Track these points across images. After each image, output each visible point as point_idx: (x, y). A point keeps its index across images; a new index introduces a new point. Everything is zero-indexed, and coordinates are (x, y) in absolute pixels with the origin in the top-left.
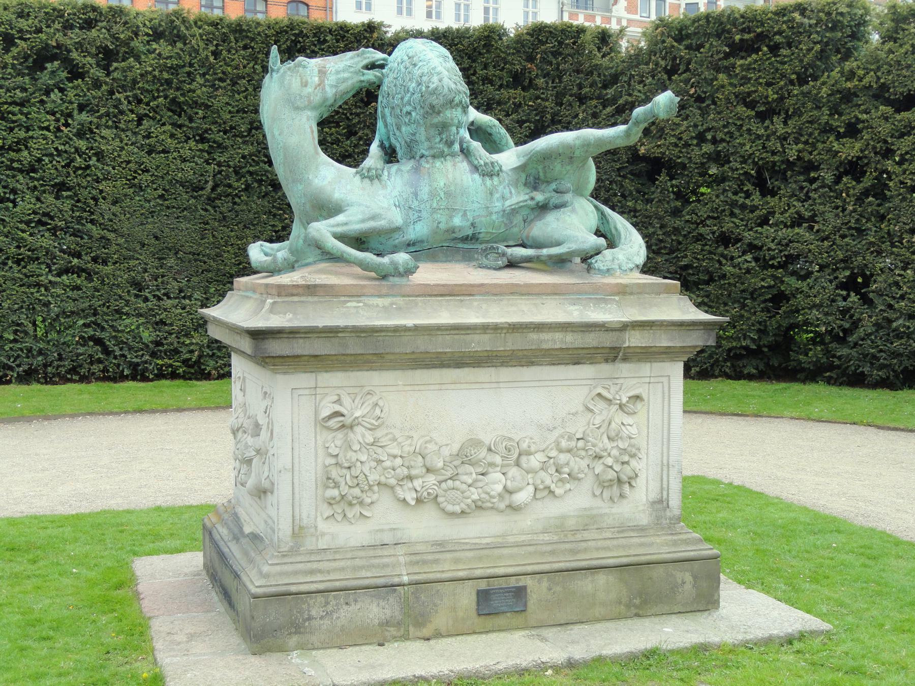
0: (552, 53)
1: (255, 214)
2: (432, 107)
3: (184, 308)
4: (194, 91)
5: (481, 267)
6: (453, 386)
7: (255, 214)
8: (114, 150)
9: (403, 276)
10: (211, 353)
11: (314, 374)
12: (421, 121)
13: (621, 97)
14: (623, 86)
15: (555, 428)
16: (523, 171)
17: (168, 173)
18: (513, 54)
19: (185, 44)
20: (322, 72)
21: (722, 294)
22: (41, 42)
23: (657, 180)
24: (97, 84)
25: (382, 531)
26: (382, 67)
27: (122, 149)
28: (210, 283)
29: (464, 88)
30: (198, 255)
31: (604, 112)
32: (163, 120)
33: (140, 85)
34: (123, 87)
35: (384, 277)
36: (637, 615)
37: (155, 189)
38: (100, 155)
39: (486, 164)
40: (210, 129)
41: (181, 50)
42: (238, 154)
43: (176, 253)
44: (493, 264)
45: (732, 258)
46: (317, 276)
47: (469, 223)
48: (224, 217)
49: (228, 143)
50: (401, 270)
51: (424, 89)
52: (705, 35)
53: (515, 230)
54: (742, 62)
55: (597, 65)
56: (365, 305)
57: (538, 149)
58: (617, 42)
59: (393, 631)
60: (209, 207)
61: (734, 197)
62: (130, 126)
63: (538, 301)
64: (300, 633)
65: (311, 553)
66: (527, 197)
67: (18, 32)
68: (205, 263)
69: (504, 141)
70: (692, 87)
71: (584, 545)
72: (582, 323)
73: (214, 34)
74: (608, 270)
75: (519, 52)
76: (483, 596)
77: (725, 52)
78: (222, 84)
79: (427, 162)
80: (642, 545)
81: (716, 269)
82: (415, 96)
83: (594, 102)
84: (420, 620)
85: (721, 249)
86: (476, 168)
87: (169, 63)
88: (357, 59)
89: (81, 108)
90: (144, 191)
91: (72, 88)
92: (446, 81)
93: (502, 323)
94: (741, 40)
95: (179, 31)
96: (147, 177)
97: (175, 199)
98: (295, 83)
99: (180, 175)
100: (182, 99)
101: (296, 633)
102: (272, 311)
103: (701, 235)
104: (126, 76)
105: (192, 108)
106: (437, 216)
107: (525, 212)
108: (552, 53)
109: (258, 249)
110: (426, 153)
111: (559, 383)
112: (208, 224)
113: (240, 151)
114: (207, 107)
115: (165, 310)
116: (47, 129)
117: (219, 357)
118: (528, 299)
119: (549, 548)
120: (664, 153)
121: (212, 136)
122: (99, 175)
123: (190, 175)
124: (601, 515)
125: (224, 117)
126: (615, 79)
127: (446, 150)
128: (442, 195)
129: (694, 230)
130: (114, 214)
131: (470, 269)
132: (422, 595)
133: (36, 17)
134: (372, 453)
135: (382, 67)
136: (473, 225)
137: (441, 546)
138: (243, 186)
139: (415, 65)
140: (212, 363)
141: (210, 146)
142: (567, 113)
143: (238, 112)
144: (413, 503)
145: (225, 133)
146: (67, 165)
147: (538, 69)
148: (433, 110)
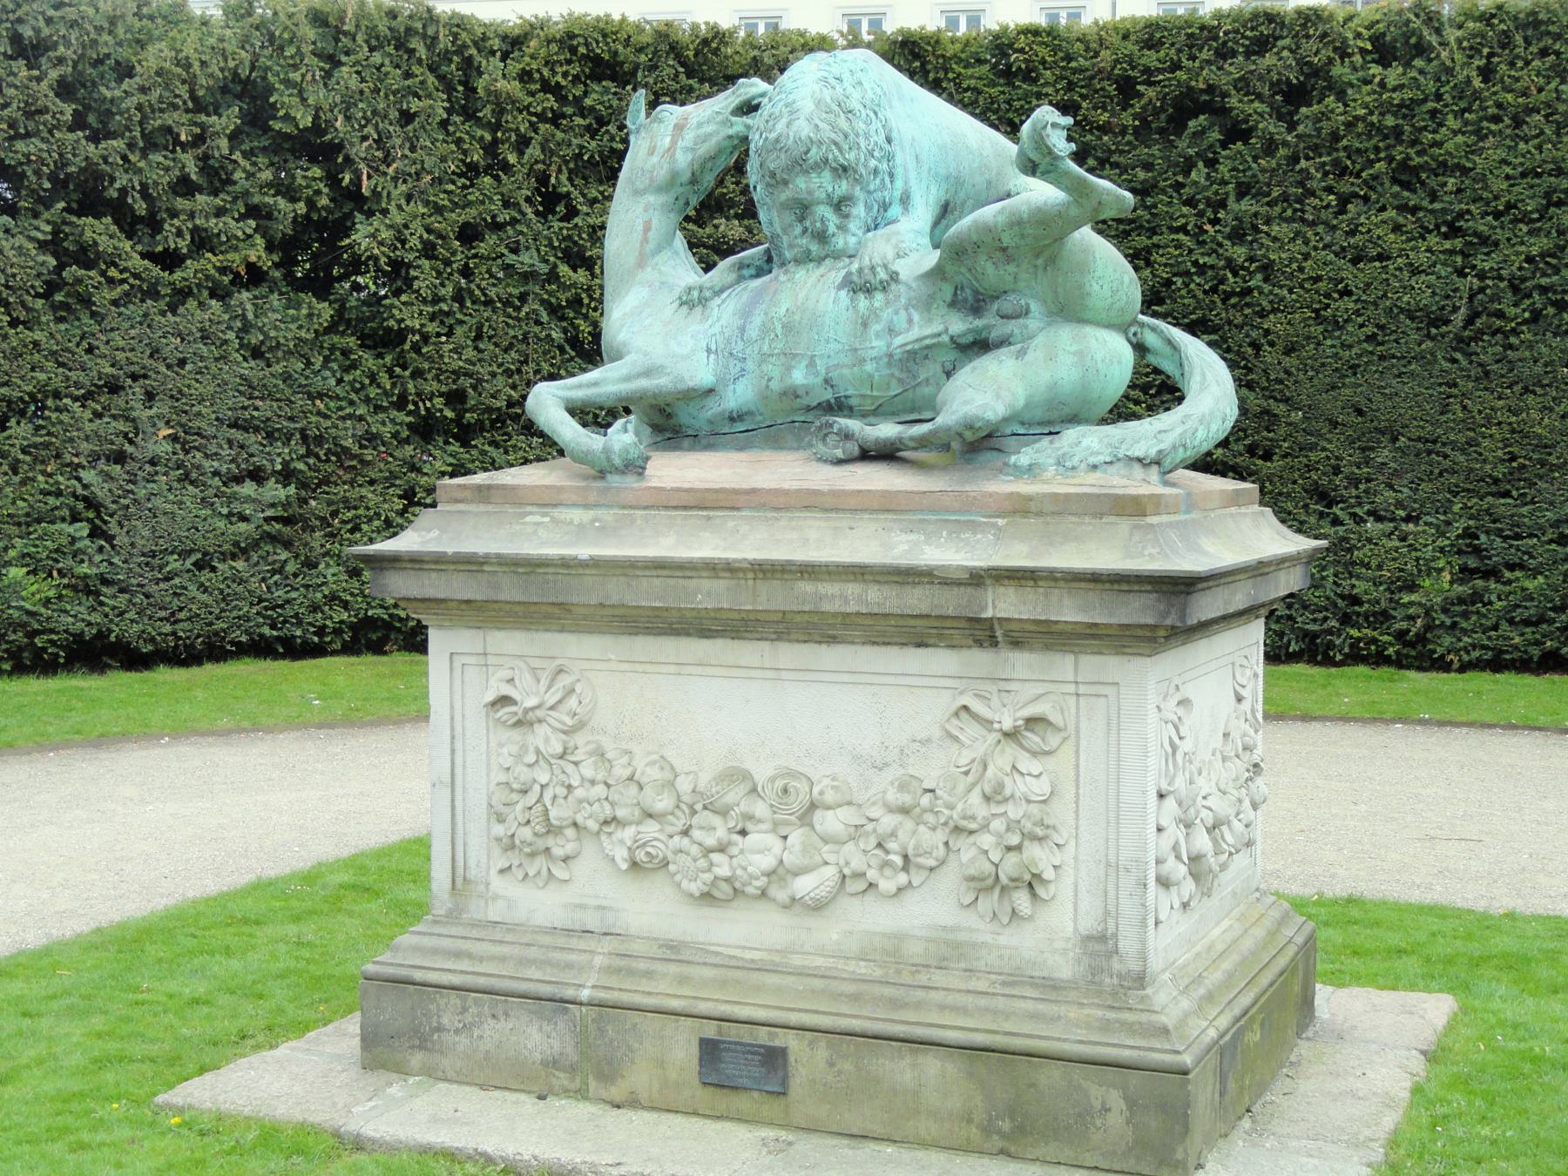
1: (1546, 365)
3: (1403, 539)
4: (1439, 144)
6: (699, 670)
7: (1546, 365)
8: (1291, 260)
10: (1448, 622)
11: (481, 632)
15: (886, 765)
17: (1385, 295)
22: (1179, 84)
24: (1270, 147)
25: (583, 907)
27: (1306, 256)
28: (1456, 494)
30: (1434, 442)
33: (1345, 142)
34: (1316, 148)
35: (602, 474)
36: (1003, 1152)
37: (1361, 326)
38: (1267, 269)
40: (1468, 212)
42: (1518, 254)
43: (1395, 439)
44: (839, 453)
47: (819, 380)
48: (1487, 374)
49: (1500, 235)
50: (617, 461)
53: (927, 390)
56: (554, 520)
59: (562, 1079)
60: (1458, 356)
62: (1324, 215)
64: (426, 1049)
65: (475, 924)
68: (1446, 456)
71: (920, 994)
73: (1483, 37)
74: (1030, 468)
76: (710, 1050)
78: (1493, 127)
80: (1034, 1016)
84: (608, 1072)
87: (1397, 97)
89: (1243, 191)
90: (1341, 328)
91: (1227, 158)
93: (739, 561)
96: (1349, 304)
97: (1396, 341)
101: (420, 1048)
104: (1319, 130)
111: (891, 680)
112: (1455, 385)
113: (1523, 248)
114: (1465, 171)
115: (1369, 540)
116: (1183, 229)
117: (1464, 631)
119: (850, 988)
122: (1264, 303)
124: (974, 945)
125: (1495, 188)
127: (814, 247)
128: (779, 331)
130: (1288, 372)
132: (609, 1028)
133: (1173, 44)
134: (557, 771)
136: (827, 381)
137: (673, 950)
138: (1527, 315)
140: (1447, 640)
143: (1523, 175)
144: (624, 866)
145: (1496, 218)
146: (1214, 290)
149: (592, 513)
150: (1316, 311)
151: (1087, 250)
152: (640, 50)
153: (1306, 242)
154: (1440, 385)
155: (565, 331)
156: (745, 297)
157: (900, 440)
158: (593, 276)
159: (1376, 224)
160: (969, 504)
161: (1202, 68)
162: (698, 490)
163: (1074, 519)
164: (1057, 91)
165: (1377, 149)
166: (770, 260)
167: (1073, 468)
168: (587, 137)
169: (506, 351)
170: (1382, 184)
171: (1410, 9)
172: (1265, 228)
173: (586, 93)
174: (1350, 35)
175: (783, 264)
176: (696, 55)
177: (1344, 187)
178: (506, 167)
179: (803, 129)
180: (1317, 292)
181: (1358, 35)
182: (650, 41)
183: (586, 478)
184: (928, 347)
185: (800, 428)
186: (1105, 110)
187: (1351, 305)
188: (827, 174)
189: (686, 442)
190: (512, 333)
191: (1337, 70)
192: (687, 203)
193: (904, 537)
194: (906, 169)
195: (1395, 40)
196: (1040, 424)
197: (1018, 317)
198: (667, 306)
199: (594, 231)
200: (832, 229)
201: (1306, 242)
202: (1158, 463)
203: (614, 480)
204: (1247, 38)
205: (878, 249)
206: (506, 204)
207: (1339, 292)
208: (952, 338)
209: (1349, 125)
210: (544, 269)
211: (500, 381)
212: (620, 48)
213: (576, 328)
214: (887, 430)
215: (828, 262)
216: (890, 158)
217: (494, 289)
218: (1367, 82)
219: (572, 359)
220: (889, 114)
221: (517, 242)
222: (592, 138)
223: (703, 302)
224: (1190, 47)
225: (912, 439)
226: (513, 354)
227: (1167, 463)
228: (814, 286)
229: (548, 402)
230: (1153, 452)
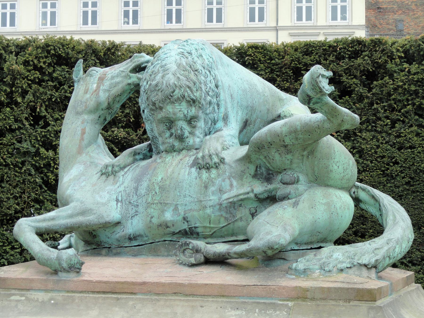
8: (372, 148)
16: (250, 162)
17: (413, 164)
27: (378, 147)
33: (393, 97)
34: (381, 99)
35: (56, 272)
37: (403, 178)
44: (193, 260)
47: (180, 218)
50: (65, 265)
53: (240, 224)
56: (27, 299)
62: (385, 128)
67: (304, 66)
74: (305, 271)
90: (394, 179)
104: (382, 91)
118: (188, 301)
127: (177, 144)
133: (317, 54)
149: (50, 295)
150: (383, 171)
151: (330, 146)
152: (79, 52)
153: (378, 141)
155: (42, 178)
156: (138, 171)
157: (228, 254)
158: (56, 153)
159: (409, 133)
160: (272, 293)
161: (330, 64)
163: (333, 303)
164: (266, 73)
165: (408, 100)
166: (151, 150)
167: (330, 271)
168: (54, 91)
169: (15, 187)
170: (410, 115)
171: (420, 40)
172: (359, 134)
173: (54, 71)
174: (394, 51)
175: (159, 153)
176: (104, 55)
177: (394, 116)
178: (17, 104)
179: (171, 79)
180: (383, 163)
181: (398, 50)
182: (84, 48)
183: (47, 273)
184: (242, 200)
185: (169, 244)
186: (287, 82)
187: (399, 169)
188: (184, 104)
189: (104, 251)
190: (17, 179)
191: (389, 66)
192: (105, 120)
193: (233, 313)
194: (226, 102)
195: (414, 53)
196: (306, 244)
197: (293, 183)
198: (94, 175)
199: (57, 133)
200: (186, 134)
201: (378, 141)
202: (375, 267)
203: (63, 275)
204: (349, 51)
205: (213, 144)
206: (16, 120)
207: (393, 162)
208: (256, 195)
209: (395, 89)
210: (33, 150)
211: (12, 201)
212: (70, 51)
213: (48, 177)
214: (220, 248)
215: (184, 152)
216: (217, 96)
217: (10, 159)
218: (402, 71)
219: (45, 191)
220: (216, 73)
221: (21, 138)
222: (57, 91)
223: (114, 173)
224: (325, 55)
225: (235, 253)
226: (18, 189)
227: (380, 267)
228: (177, 165)
229: (26, 229)
230: (373, 261)
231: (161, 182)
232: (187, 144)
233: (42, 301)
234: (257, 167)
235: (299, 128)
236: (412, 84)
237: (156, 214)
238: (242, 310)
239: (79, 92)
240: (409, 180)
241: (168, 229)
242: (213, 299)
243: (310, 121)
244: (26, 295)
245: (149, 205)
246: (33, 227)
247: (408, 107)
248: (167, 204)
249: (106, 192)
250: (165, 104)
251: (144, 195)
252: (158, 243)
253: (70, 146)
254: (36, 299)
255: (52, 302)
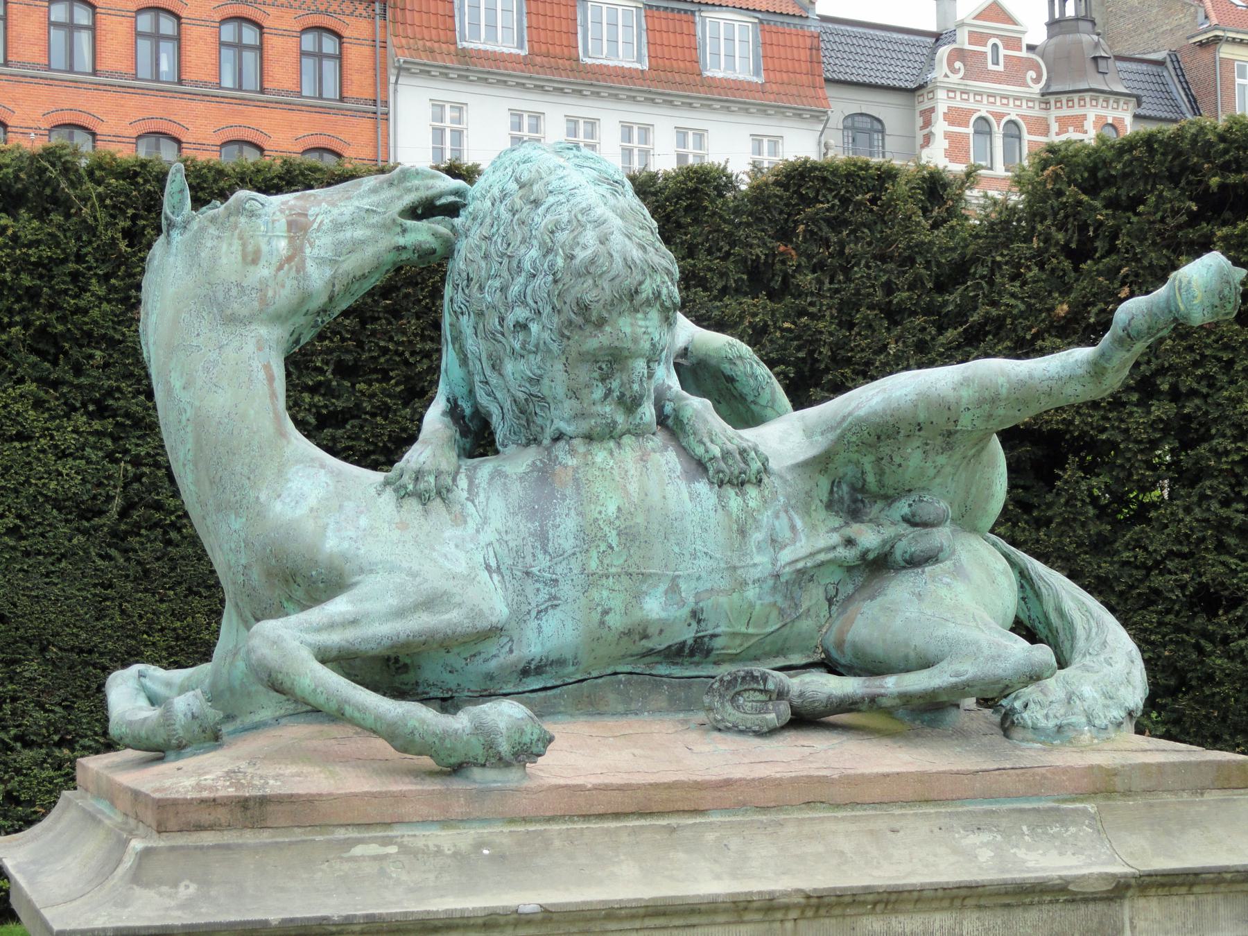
0: (828, 221)
2: (583, 308)
4: (85, 312)
5: (719, 728)
9: (508, 765)
12: (555, 347)
13: (975, 308)
14: (978, 286)
16: (824, 471)
17: (27, 481)
18: (748, 225)
19: (68, 216)
20: (298, 227)
21: (1208, 717)
23: (1059, 477)
26: (452, 210)
29: (665, 259)
30: (90, 652)
31: (941, 339)
32: (20, 372)
35: (457, 769)
39: (726, 454)
40: (119, 389)
41: (59, 227)
43: (43, 649)
44: (752, 720)
45: (1226, 640)
46: (270, 770)
47: (685, 612)
48: (146, 572)
50: (505, 748)
51: (560, 262)
52: (1146, 177)
53: (806, 625)
54: (1225, 230)
55: (923, 243)
56: (404, 849)
57: (862, 412)
58: (960, 197)
60: (113, 552)
61: (1224, 512)
63: (882, 824)
66: (835, 538)
69: (765, 398)
70: (1123, 284)
72: (1005, 883)
73: (127, 196)
74: (1060, 728)
75: (760, 220)
77: (1189, 212)
79: (572, 452)
81: (1193, 662)
82: (537, 282)
83: (919, 321)
85: (1200, 621)
86: (699, 466)
88: (386, 194)
92: (618, 241)
93: (785, 894)
94: (1223, 186)
95: (55, 190)
97: (42, 535)
98: (228, 255)
99: (53, 485)
100: (60, 328)
102: (137, 877)
103: (1157, 592)
105: (81, 346)
106: (601, 595)
107: (831, 577)
108: (828, 221)
109: (133, 684)
110: (569, 429)
112: (110, 586)
114: (112, 343)
115: (18, 771)
118: (855, 819)
120: (1071, 422)
121: (122, 403)
123: (75, 485)
126: (959, 272)
127: (620, 418)
128: (613, 539)
129: (1141, 581)
131: (693, 736)
135: (452, 210)
136: (695, 615)
139: (536, 203)
141: (117, 424)
142: (864, 343)
147: (800, 255)
148: (586, 317)
154: (95, 586)
162: (639, 787)
231: (617, 517)
232: (638, 420)
233: (455, 854)
234: (833, 483)
235: (1004, 391)
236: (23, 269)
237: (617, 602)
238: (991, 831)
239: (214, 259)
240: (18, 521)
241: (644, 642)
242: (903, 811)
243: (1064, 368)
244: (399, 840)
245: (592, 580)
246: (310, 645)
247: (13, 330)
248: (650, 575)
249: (452, 545)
250: (615, 315)
251: (574, 554)
252: (600, 681)
253: (252, 412)
254: (433, 848)
255: (486, 852)
